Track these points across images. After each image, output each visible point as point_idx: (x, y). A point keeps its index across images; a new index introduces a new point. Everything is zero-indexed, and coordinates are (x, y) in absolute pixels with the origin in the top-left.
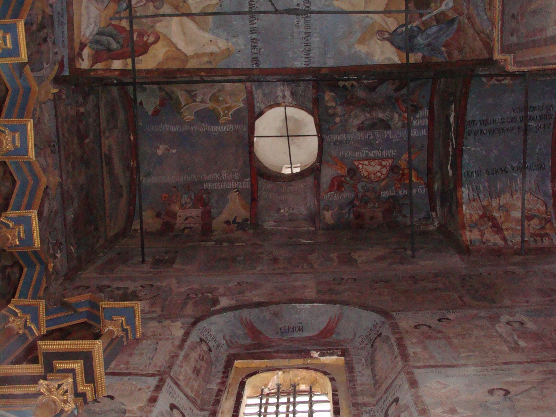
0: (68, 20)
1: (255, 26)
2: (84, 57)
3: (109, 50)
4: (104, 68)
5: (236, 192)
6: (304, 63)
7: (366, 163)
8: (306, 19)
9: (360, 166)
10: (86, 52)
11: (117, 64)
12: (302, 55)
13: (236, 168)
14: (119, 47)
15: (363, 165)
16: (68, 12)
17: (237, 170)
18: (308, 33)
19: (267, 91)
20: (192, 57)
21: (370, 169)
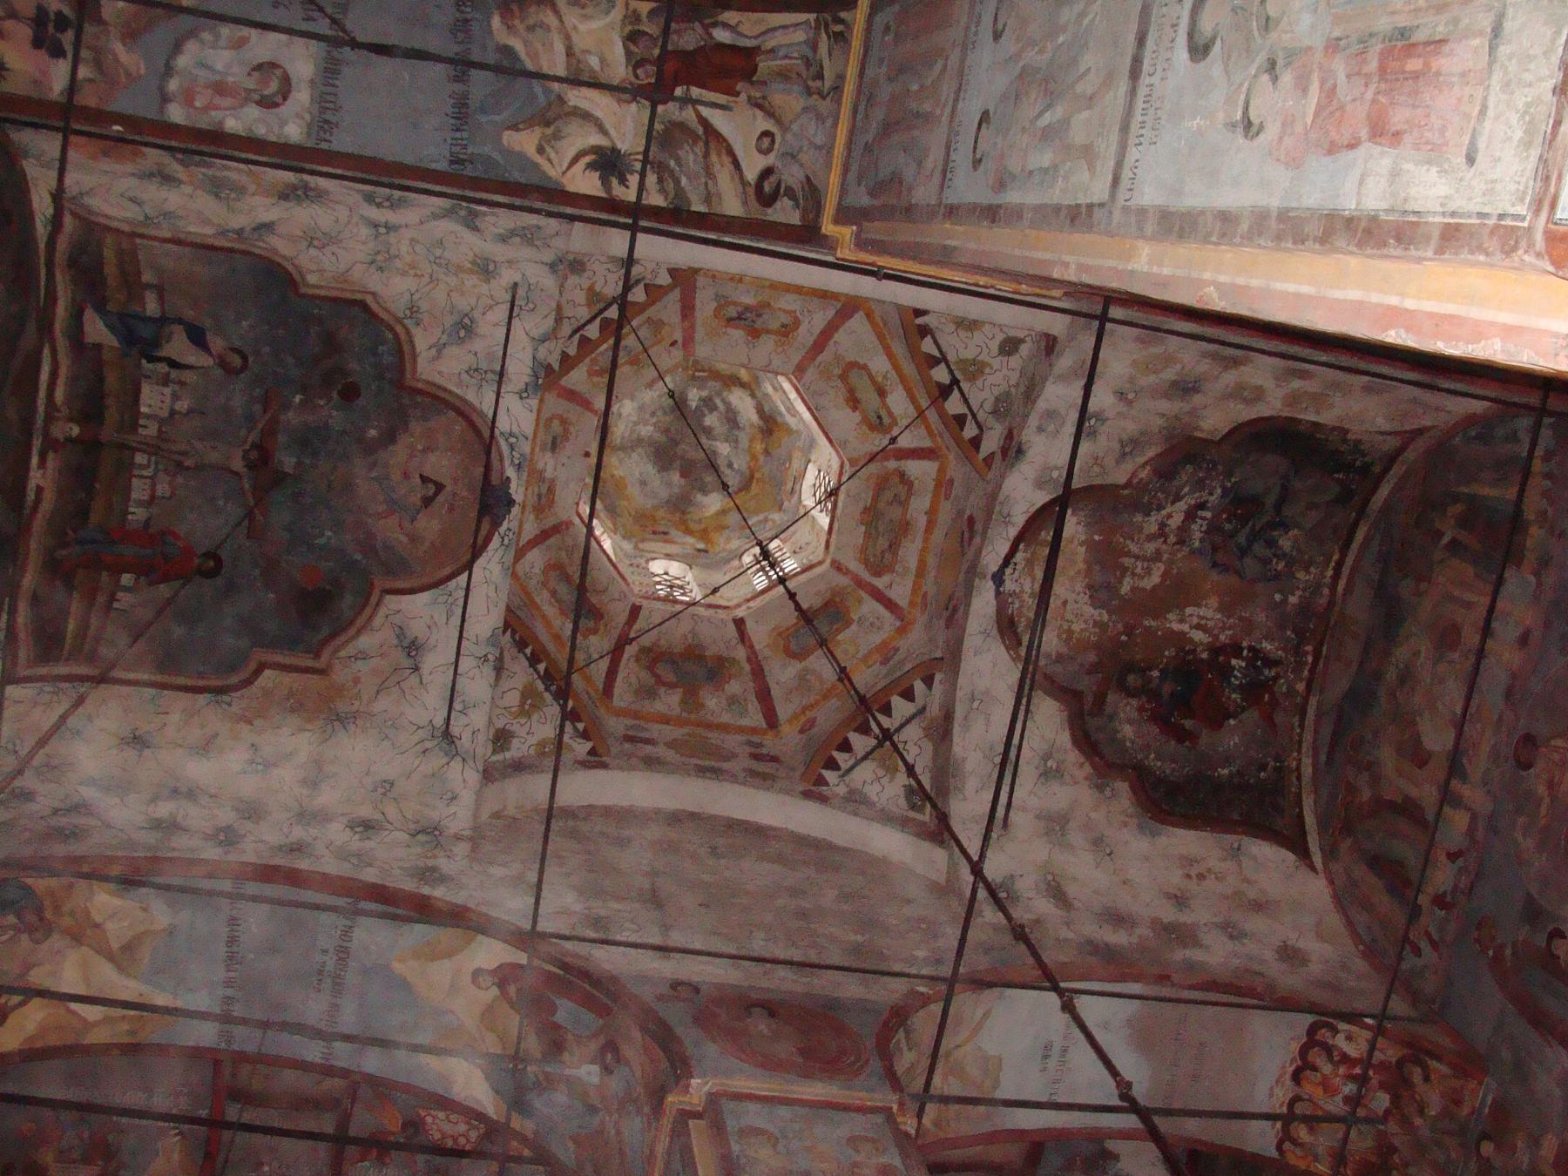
5: (176, 1135)
7: (442, 1115)
9: (429, 1120)
15: (434, 1117)
21: (448, 1128)
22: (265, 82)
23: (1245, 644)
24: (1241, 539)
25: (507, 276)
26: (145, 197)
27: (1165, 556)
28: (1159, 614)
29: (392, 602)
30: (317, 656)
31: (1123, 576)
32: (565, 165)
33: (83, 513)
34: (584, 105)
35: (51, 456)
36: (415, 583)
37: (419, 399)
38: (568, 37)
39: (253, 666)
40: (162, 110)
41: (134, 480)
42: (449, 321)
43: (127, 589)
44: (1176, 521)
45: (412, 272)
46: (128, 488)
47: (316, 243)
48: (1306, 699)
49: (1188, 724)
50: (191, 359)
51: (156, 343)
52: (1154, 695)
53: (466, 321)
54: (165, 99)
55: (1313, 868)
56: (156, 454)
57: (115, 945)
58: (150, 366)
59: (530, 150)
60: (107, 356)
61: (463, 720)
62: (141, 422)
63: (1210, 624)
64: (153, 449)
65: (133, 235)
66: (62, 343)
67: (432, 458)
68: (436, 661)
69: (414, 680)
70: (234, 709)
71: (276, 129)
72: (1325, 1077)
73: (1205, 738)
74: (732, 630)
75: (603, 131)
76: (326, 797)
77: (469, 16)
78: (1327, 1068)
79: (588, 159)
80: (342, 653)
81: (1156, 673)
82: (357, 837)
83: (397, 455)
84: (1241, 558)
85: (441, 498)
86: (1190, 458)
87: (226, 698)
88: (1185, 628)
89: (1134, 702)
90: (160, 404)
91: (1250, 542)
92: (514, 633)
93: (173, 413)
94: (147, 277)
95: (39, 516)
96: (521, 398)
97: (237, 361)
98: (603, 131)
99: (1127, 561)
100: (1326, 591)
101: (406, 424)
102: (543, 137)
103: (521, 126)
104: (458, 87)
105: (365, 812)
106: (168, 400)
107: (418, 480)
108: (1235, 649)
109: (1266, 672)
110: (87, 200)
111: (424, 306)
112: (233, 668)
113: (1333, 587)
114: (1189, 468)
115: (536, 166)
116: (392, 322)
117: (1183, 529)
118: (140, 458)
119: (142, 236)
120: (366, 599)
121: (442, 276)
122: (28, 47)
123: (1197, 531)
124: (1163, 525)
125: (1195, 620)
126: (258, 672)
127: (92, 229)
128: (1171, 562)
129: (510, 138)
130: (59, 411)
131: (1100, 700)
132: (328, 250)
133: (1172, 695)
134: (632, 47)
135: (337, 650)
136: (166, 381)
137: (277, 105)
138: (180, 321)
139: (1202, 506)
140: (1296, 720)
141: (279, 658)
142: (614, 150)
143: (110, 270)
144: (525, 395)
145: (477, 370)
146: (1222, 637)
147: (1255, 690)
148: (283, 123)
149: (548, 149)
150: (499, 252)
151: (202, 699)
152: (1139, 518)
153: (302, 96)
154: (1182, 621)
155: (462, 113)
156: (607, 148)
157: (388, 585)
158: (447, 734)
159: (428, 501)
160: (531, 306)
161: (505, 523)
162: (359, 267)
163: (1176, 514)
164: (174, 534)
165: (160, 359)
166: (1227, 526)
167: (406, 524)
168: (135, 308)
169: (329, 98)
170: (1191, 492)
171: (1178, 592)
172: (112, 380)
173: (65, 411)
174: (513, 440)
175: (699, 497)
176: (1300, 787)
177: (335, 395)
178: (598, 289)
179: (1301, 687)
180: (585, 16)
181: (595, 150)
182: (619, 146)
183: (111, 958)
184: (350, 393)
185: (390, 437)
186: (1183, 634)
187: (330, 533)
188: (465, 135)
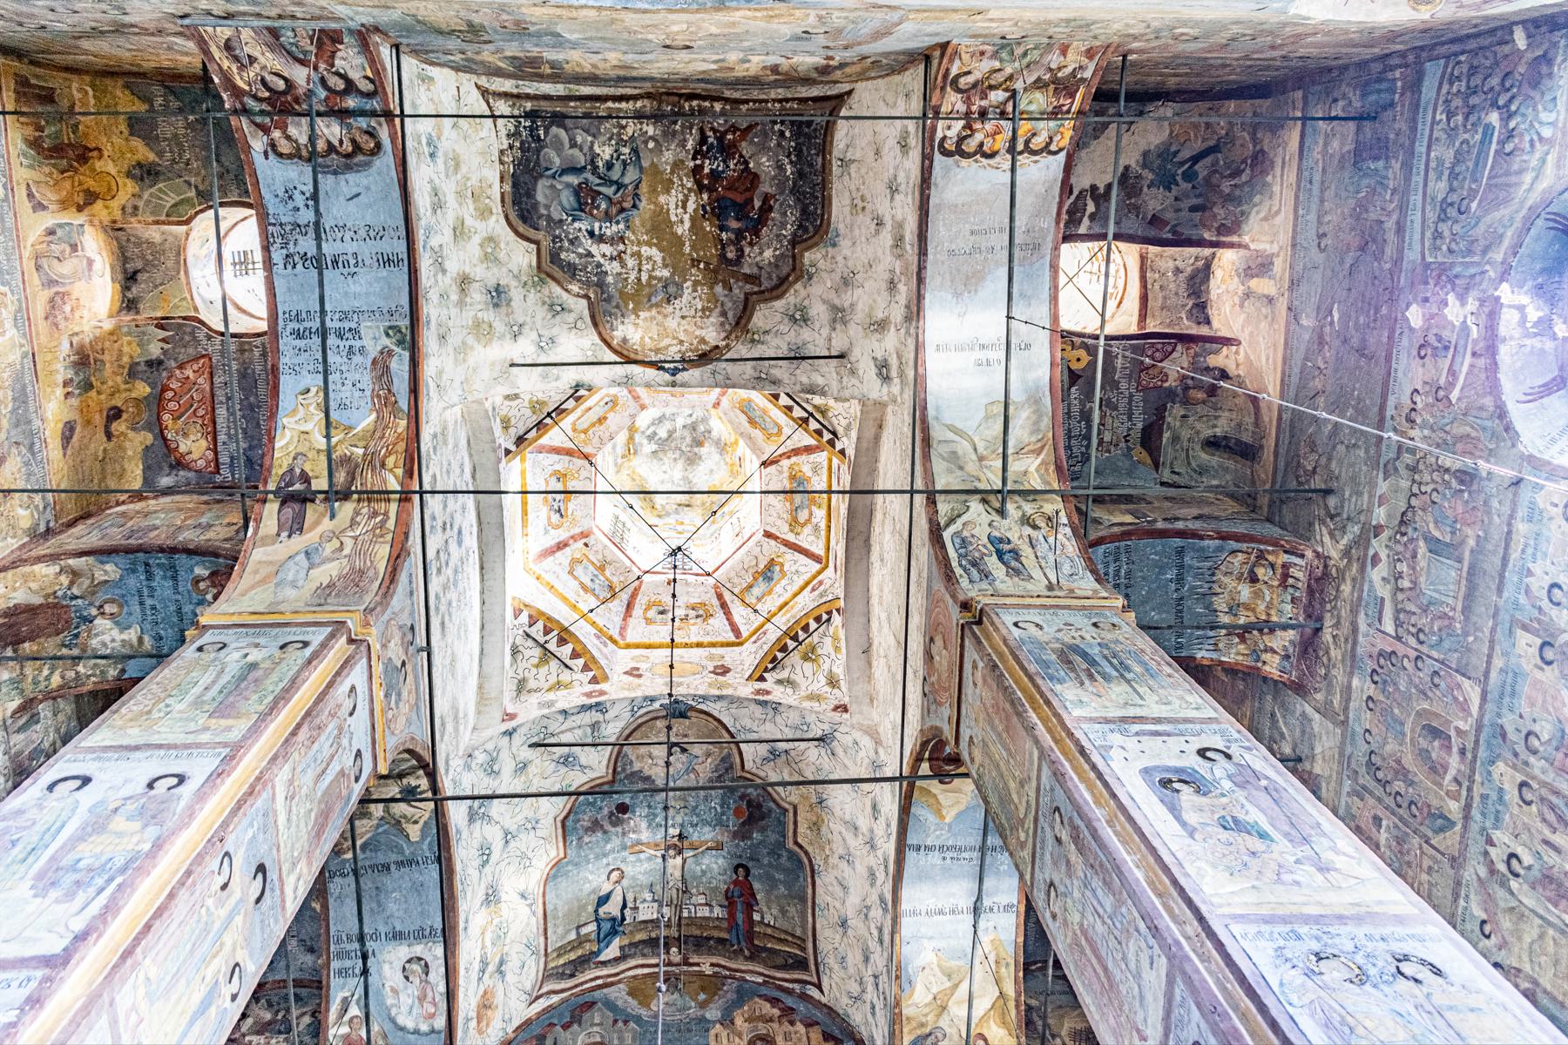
22: (413, 972)
23: (692, 164)
24: (609, 191)
25: (527, 754)
26: (519, 964)
27: (636, 248)
28: (679, 241)
29: (749, 765)
31: (654, 278)
33: (721, 941)
40: (439, 1032)
42: (563, 770)
44: (607, 249)
48: (726, 100)
49: (757, 204)
50: (620, 899)
51: (613, 919)
52: (739, 234)
54: (433, 1031)
55: (850, 93)
57: (948, 984)
59: (418, 827)
60: (626, 942)
63: (681, 197)
65: (546, 955)
72: (987, 136)
73: (766, 187)
74: (772, 469)
78: (979, 137)
81: (724, 236)
84: (626, 186)
86: (555, 258)
88: (687, 217)
89: (747, 250)
91: (612, 183)
92: (766, 670)
94: (573, 936)
97: (615, 875)
99: (644, 277)
100: (639, 104)
104: (393, 868)
108: (697, 170)
109: (711, 140)
112: (800, 861)
113: (635, 98)
114: (563, 256)
117: (612, 241)
118: (685, 914)
120: (747, 780)
123: (610, 230)
124: (612, 259)
125: (680, 210)
126: (801, 847)
127: (548, 975)
128: (639, 243)
131: (751, 279)
133: (738, 220)
136: (636, 908)
138: (596, 911)
139: (591, 234)
140: (744, 108)
141: (791, 834)
143: (573, 956)
146: (689, 185)
147: (727, 150)
151: (818, 882)
152: (610, 279)
153: (418, 950)
154: (682, 222)
163: (600, 251)
164: (727, 891)
166: (603, 206)
168: (593, 936)
170: (581, 244)
171: (660, 228)
175: (715, 434)
176: (793, 99)
178: (536, 661)
179: (718, 107)
183: (956, 986)
186: (692, 219)
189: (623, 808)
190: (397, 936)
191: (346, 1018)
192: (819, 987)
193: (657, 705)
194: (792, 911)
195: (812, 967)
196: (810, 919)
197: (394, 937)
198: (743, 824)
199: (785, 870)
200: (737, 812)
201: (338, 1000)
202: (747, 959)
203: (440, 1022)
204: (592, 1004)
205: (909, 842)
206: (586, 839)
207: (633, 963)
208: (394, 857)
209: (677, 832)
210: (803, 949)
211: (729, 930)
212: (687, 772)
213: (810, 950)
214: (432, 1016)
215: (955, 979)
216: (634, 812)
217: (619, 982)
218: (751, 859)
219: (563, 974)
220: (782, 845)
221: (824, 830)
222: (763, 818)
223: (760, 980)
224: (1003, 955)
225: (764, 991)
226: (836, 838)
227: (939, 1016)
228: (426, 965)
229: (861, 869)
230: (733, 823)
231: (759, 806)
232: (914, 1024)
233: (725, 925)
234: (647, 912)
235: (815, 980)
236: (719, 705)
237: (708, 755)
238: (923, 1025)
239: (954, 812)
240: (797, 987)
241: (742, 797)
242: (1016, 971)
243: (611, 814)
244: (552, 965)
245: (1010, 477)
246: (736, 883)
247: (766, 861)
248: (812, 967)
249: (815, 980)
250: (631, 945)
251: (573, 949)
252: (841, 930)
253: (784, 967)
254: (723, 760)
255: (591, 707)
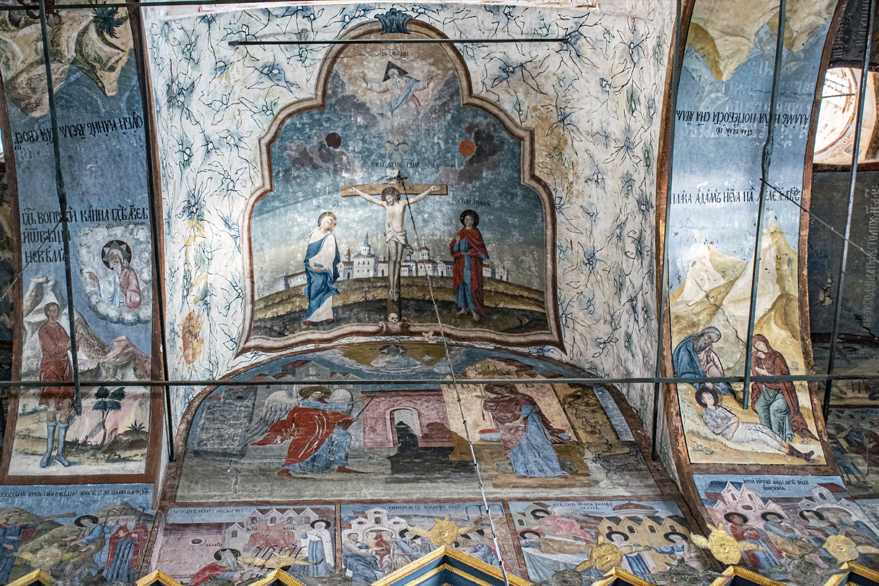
0: (769, 473)
1: (742, 195)
2: (807, 451)
3: (787, 411)
4: (813, 420)
6: (803, 125)
8: (741, 119)
10: (800, 446)
11: (804, 400)
12: (792, 126)
13: (864, 192)
14: (780, 395)
16: (758, 473)
17: (867, 190)
18: (761, 117)
19: (545, 31)
20: (783, 288)
22: (114, 257)
25: (226, 52)
26: (224, 303)
29: (477, 89)
30: (522, 139)
32: (117, 51)
33: (445, 305)
34: (73, 46)
35: (412, 329)
36: (461, 72)
37: (329, 92)
38: (31, 65)
39: (534, 184)
40: (146, 322)
41: (420, 275)
42: (268, 83)
43: (493, 273)
45: (238, 117)
46: (424, 278)
47: (231, 187)
50: (332, 250)
51: (325, 274)
53: (265, 71)
54: (139, 321)
56: (400, 263)
57: (722, 282)
58: (341, 274)
59: (114, 75)
60: (340, 303)
61: (554, 28)
62: (380, 275)
64: (397, 265)
65: (253, 302)
66: (335, 332)
67: (370, 75)
68: (515, 54)
69: (529, 66)
70: (563, 195)
71: (143, 246)
75: (85, 31)
76: (616, 129)
77: (39, 133)
79: (108, 37)
80: (517, 121)
82: (638, 107)
83: (373, 99)
85: (398, 64)
87: (557, 201)
90: (366, 265)
93: (370, 255)
94: (281, 287)
95: (453, 332)
96: (315, 19)
97: (326, 220)
98: (85, 31)
101: (349, 97)
102: (102, 69)
103: (100, 85)
104: (87, 131)
105: (623, 98)
106: (361, 260)
107: (388, 82)
110: (235, 335)
111: (261, 102)
112: (538, 198)
115: (123, 69)
116: (278, 122)
119: (252, 296)
120: (481, 108)
121: (236, 97)
122: (119, 413)
126: (539, 181)
127: (256, 327)
129: (111, 90)
130: (382, 327)
132: (235, 178)
134: (22, 22)
135: (516, 126)
136: (349, 263)
137: (128, 248)
138: (306, 261)
141: (527, 167)
142: (95, 21)
143: (281, 310)
144: (312, 17)
145: (300, 55)
148: (138, 241)
149: (110, 64)
150: (207, 63)
151: (560, 218)
153: (118, 232)
155: (104, 125)
156: (96, 26)
157: (466, 92)
158: (564, 40)
159: (402, 73)
160: (244, 28)
161: (408, 13)
162: (244, 153)
165: (335, 269)
167: (421, 85)
168: (304, 291)
169: (115, 215)
172: (354, 298)
173: (381, 323)
174: (347, 19)
177: (338, 150)
180: (14, 55)
181: (100, 34)
182: (92, 18)
183: (732, 283)
184: (334, 140)
185: (361, 108)
187: (436, 138)
188: (117, 121)
189: (334, 140)
190: (95, 216)
191: (41, 306)
192: (561, 346)
193: (371, 16)
194: (528, 260)
195: (552, 323)
196: (550, 266)
197: (91, 218)
198: (471, 162)
199: (522, 213)
200: (464, 148)
201: (32, 287)
202: (476, 324)
203: (146, 312)
204: (306, 362)
205: (679, 108)
206: (295, 173)
207: (347, 328)
208: (87, 118)
209: (396, 173)
210: (541, 304)
211: (455, 292)
212: (406, 99)
213: (550, 304)
214: (138, 305)
215: (731, 276)
216: (346, 146)
217: (333, 347)
218: (481, 203)
219: (271, 329)
220: (516, 181)
221: (567, 152)
222: (493, 152)
223: (491, 346)
224: (785, 250)
225: (497, 354)
226: (583, 157)
227: (713, 314)
228: (128, 250)
229: (613, 183)
230: (459, 163)
231: (490, 137)
232: (684, 323)
233: (450, 285)
234: (363, 270)
235: (555, 338)
236: (442, 15)
237: (430, 78)
238: (694, 325)
239: (732, 67)
240: (533, 350)
241: (469, 130)
242: (800, 269)
243: (321, 146)
244: (260, 316)
245: (647, 375)
246: (463, 234)
247: (497, 205)
248: (552, 323)
249: (555, 338)
250: (345, 306)
251: (281, 302)
252: (586, 269)
253: (520, 329)
254: (447, 84)
255: (296, 11)
